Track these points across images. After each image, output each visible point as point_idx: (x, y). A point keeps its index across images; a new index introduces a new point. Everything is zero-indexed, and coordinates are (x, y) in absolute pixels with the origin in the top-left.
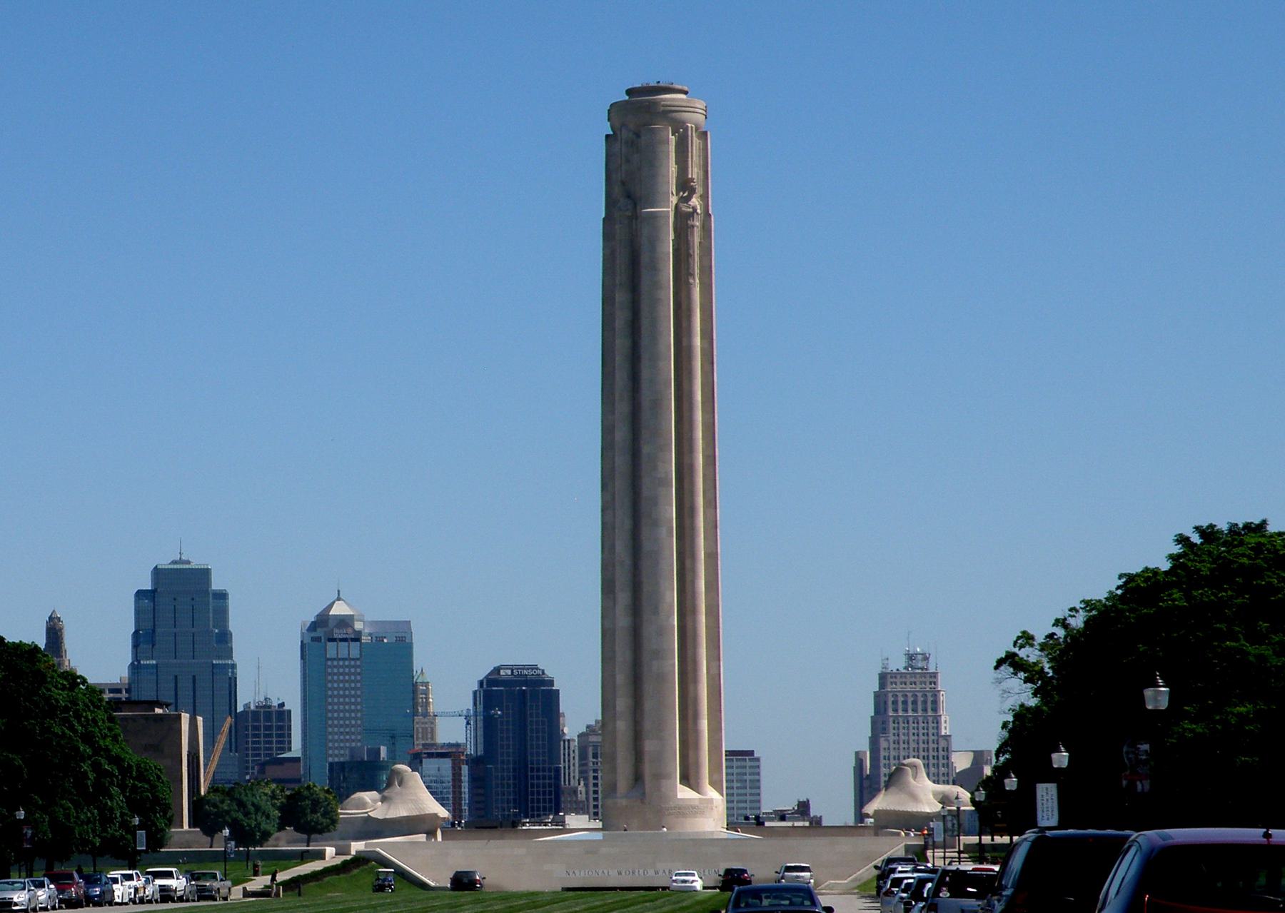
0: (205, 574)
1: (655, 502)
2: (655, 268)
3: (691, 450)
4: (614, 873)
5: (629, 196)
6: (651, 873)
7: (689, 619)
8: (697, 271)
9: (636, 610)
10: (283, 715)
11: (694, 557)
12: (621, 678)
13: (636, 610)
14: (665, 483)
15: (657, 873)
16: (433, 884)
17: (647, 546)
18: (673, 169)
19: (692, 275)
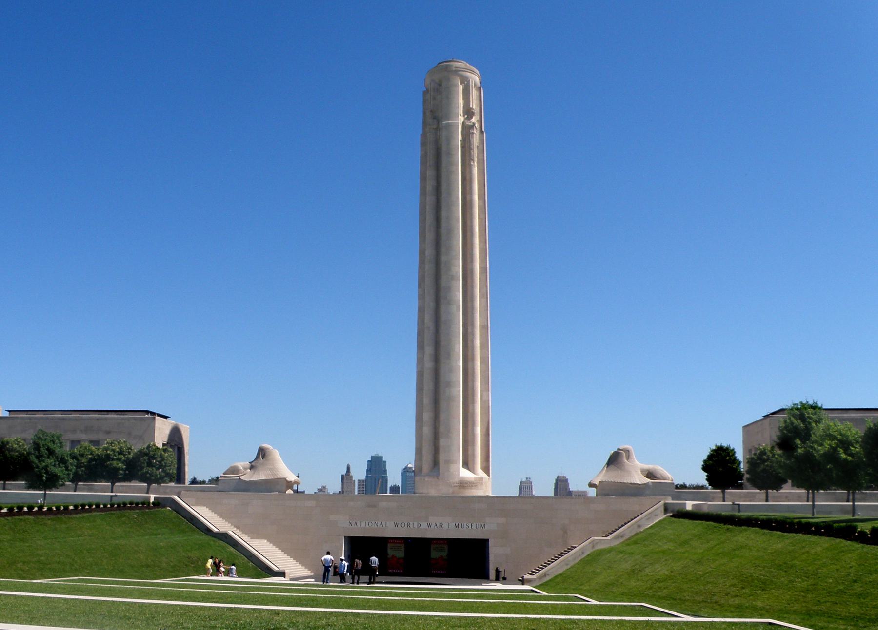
0: (382, 457)
1: (449, 289)
2: (449, 154)
3: (472, 261)
4: (391, 525)
5: (434, 118)
6: (424, 525)
7: (470, 364)
8: (475, 159)
9: (437, 359)
10: (399, 487)
11: (473, 325)
12: (427, 401)
13: (437, 359)
14: (454, 278)
15: (429, 526)
16: (215, 530)
17: (443, 317)
18: (461, 102)
19: (473, 160)
